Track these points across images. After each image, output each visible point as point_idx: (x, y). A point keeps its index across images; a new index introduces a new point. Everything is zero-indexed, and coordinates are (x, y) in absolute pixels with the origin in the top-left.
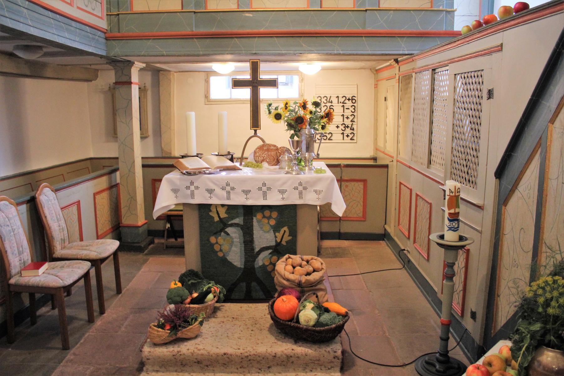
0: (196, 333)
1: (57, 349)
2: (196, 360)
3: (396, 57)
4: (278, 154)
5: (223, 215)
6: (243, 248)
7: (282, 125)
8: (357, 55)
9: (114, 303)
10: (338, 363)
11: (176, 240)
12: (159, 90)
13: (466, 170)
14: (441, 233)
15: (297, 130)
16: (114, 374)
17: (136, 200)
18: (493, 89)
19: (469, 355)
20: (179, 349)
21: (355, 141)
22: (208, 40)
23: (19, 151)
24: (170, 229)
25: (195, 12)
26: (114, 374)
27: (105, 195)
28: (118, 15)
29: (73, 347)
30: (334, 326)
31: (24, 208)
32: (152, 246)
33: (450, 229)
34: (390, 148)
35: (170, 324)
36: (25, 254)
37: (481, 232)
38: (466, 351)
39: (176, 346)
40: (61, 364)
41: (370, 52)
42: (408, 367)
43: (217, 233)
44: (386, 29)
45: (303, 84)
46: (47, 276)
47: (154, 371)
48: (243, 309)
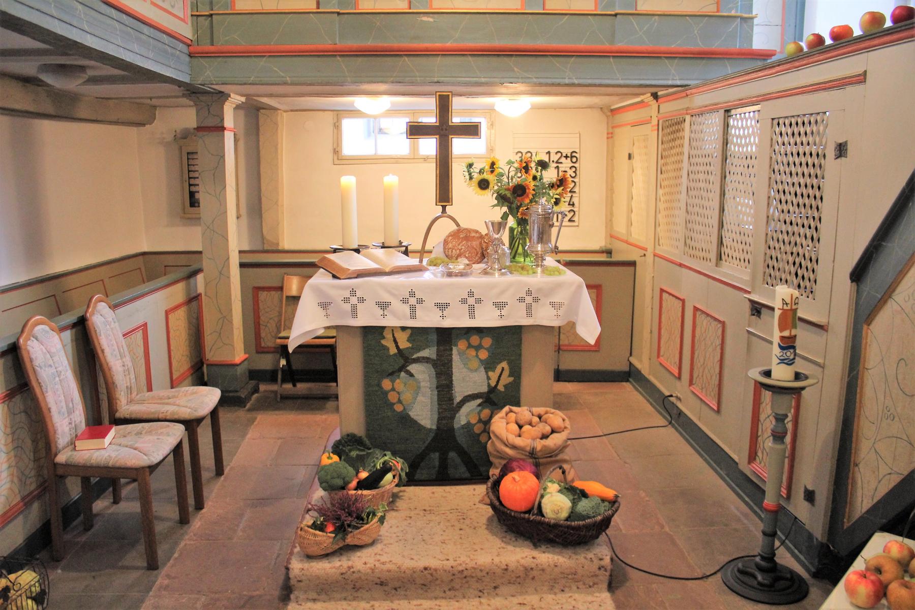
0: (374, 536)
1: (137, 568)
2: (378, 581)
3: (654, 90)
4: (484, 245)
5: (404, 344)
6: (436, 397)
7: (489, 197)
8: (600, 85)
9: (215, 491)
10: (604, 577)
11: (294, 385)
12: (258, 141)
13: (793, 270)
14: (766, 368)
15: (514, 206)
16: (243, 607)
17: (231, 322)
18: (846, 142)
19: (802, 557)
20: (350, 563)
21: (576, 224)
22: (360, 59)
23: (33, 238)
24: (286, 368)
25: (339, 13)
26: (243, 607)
27: (182, 313)
28: (211, 15)
29: (165, 564)
30: (599, 518)
31: (68, 335)
32: (256, 395)
33: (782, 361)
34: (640, 233)
35: (334, 524)
36: (77, 412)
37: (822, 366)
38: (796, 551)
39: (344, 558)
40: (151, 593)
41: (621, 82)
42: (710, 579)
43: (392, 374)
44: (647, 45)
45: (493, 131)
46: (113, 449)
47: (308, 600)
48: (436, 495)
